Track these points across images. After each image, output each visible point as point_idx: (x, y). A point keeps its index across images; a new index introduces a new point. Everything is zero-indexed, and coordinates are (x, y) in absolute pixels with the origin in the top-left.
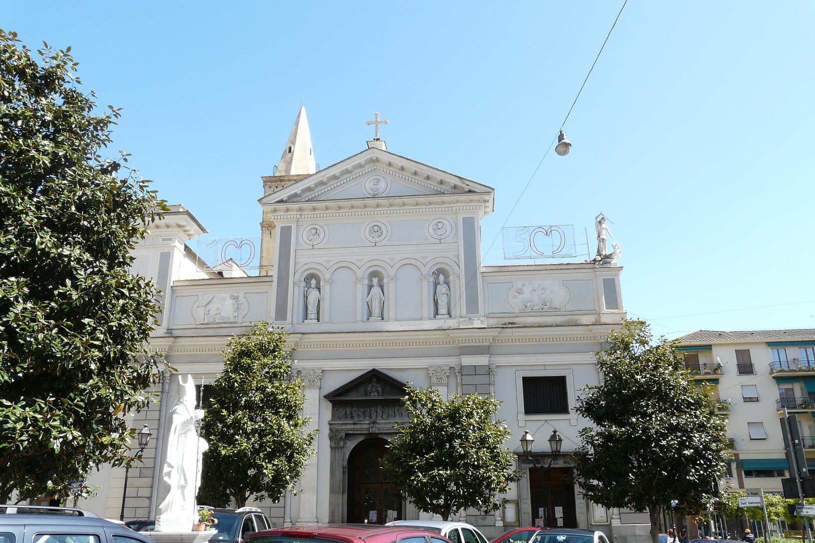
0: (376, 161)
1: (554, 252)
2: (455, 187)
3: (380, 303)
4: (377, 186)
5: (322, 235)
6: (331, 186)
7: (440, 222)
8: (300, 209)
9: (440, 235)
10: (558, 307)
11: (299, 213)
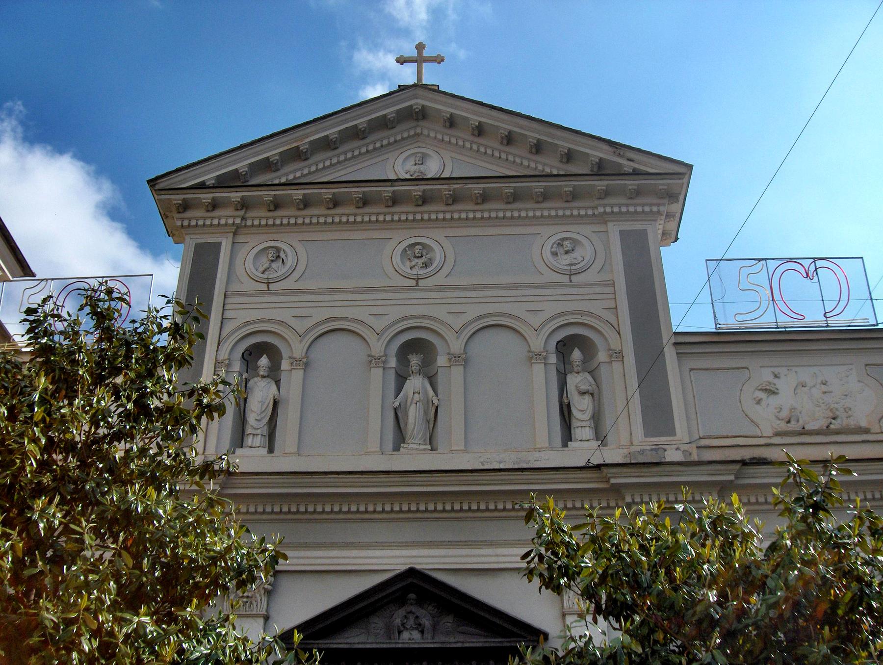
0: (421, 117)
1: (828, 315)
2: (601, 163)
3: (426, 413)
4: (422, 168)
5: (290, 262)
6: (190, 219)
7: (566, 239)
8: (244, 205)
9: (571, 265)
10: (864, 424)
11: (242, 213)
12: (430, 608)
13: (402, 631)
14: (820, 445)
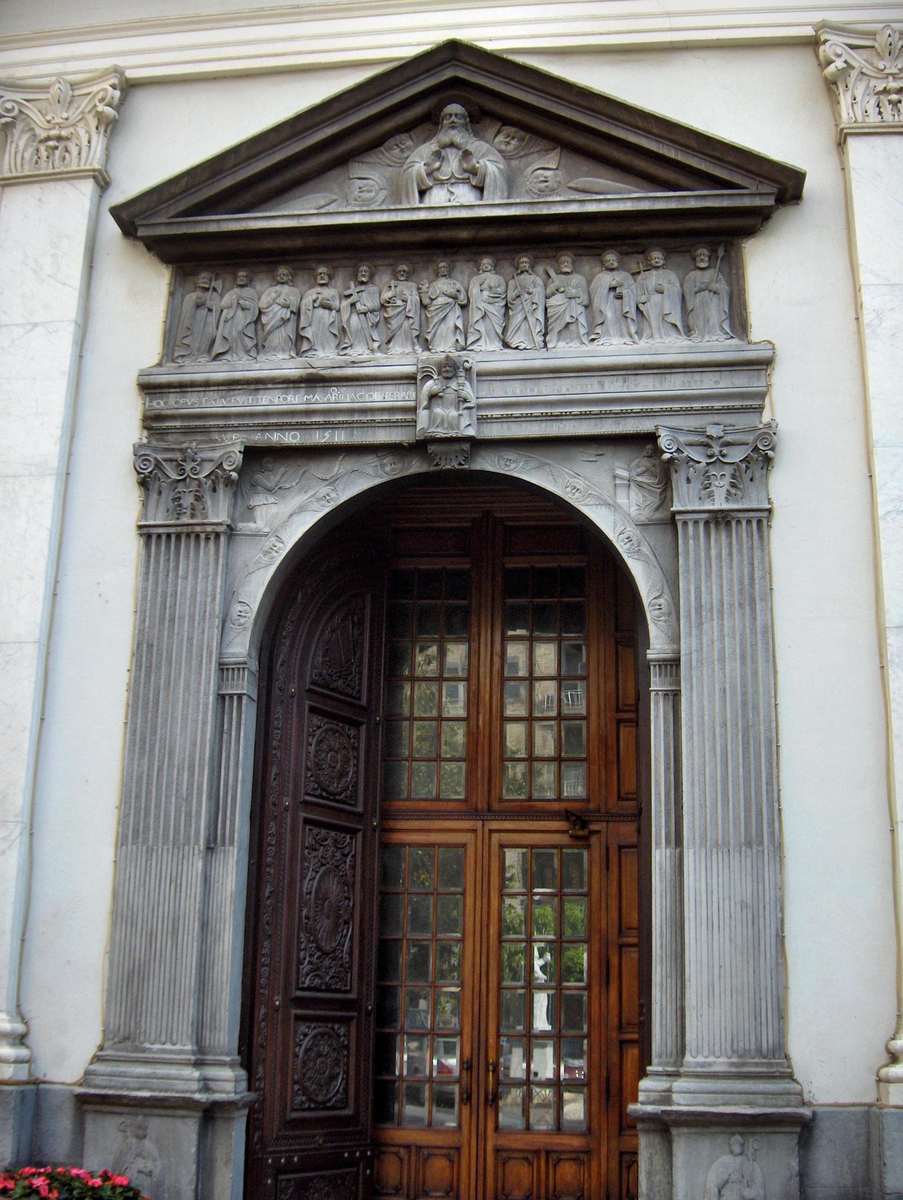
12: (500, 138)
13: (431, 188)
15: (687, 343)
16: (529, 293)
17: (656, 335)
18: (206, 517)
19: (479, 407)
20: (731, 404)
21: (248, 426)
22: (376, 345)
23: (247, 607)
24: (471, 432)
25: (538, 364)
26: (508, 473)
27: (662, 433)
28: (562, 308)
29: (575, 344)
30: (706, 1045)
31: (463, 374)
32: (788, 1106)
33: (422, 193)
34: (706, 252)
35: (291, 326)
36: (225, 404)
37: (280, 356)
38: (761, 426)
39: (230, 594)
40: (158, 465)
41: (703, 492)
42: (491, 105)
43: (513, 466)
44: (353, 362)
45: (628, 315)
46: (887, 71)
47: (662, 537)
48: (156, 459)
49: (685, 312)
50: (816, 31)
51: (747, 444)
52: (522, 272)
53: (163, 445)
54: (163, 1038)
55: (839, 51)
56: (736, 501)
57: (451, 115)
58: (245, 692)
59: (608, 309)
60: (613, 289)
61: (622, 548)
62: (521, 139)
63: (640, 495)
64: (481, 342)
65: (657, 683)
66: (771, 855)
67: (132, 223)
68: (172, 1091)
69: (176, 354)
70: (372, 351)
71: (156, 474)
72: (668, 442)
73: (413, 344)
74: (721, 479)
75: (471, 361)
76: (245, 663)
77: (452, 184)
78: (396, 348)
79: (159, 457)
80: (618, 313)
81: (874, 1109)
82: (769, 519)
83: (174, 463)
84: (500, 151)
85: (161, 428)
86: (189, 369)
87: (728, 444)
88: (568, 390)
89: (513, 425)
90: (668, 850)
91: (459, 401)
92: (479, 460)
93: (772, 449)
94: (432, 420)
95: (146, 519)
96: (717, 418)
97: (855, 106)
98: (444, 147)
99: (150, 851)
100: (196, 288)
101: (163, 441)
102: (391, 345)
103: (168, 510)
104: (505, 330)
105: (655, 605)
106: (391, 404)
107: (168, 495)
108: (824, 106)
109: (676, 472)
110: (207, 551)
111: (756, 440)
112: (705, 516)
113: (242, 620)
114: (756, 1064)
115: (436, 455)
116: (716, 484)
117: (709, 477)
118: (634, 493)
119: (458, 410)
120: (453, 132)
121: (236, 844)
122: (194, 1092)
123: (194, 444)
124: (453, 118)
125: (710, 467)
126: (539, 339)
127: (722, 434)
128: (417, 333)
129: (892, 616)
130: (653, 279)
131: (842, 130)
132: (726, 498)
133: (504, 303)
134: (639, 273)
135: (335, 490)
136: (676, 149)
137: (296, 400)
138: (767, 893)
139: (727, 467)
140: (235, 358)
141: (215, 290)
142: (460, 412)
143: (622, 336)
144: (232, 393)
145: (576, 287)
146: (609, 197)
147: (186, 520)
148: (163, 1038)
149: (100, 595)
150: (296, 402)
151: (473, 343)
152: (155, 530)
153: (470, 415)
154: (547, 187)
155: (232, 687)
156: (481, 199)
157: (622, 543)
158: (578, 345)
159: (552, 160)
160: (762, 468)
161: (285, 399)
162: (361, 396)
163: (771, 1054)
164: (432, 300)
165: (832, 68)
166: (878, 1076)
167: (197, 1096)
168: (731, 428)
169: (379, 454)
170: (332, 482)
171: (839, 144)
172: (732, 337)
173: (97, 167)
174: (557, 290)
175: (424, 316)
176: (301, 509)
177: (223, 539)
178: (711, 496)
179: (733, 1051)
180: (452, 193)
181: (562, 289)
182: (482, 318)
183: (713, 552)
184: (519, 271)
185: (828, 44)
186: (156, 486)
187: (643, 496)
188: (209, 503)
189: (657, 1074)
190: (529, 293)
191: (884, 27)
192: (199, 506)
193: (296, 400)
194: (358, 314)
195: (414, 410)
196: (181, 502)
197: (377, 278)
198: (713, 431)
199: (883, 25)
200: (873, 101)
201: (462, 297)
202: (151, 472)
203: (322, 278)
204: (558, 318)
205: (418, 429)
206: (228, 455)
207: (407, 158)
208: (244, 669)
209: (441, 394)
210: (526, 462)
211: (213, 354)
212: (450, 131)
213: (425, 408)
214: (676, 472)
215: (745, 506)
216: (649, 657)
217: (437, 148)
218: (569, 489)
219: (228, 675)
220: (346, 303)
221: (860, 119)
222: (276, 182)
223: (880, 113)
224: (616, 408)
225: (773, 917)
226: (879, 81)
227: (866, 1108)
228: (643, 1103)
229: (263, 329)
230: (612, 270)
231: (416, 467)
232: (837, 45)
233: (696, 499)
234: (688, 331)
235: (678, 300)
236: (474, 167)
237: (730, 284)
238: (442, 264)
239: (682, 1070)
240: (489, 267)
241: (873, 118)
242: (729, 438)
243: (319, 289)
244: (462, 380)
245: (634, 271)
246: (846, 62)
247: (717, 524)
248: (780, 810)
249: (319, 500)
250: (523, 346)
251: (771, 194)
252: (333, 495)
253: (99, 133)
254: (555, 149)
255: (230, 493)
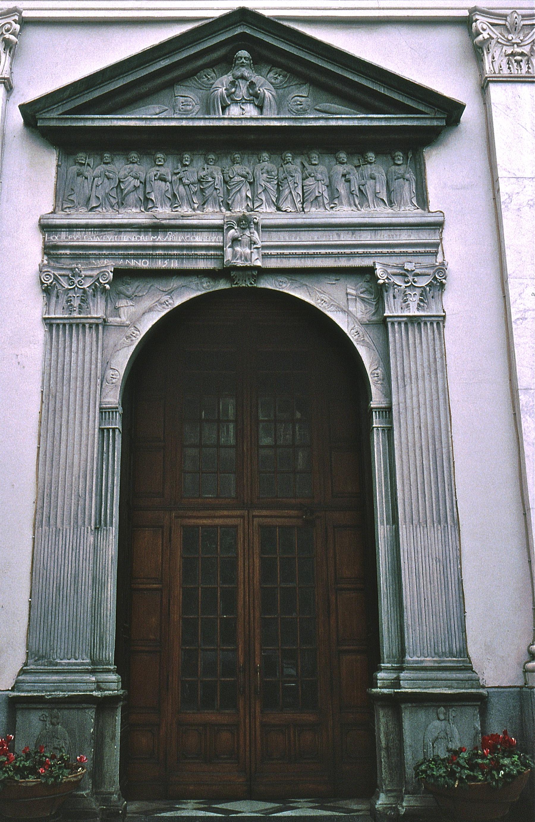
12: (271, 74)
13: (229, 105)
14: (501, 300)
15: (390, 211)
16: (292, 176)
17: (371, 205)
18: (90, 313)
19: (264, 247)
20: (418, 250)
21: (115, 254)
22: (196, 206)
23: (117, 372)
24: (259, 263)
25: (299, 221)
26: (281, 290)
27: (378, 266)
28: (314, 186)
29: (322, 210)
30: (419, 649)
31: (253, 226)
32: (472, 688)
33: (224, 109)
34: (401, 154)
35: (141, 191)
36: (99, 240)
37: (134, 210)
38: (437, 264)
39: (106, 364)
40: (56, 278)
41: (404, 304)
42: (266, 53)
43: (284, 285)
44: (182, 216)
45: (354, 192)
46: (514, 41)
47: (374, 332)
48: (54, 274)
49: (389, 192)
50: (470, 13)
51: (430, 275)
52: (287, 163)
53: (58, 265)
54: (69, 656)
55: (485, 27)
56: (423, 310)
57: (241, 58)
58: (117, 427)
59: (342, 188)
60: (344, 175)
61: (353, 338)
62: (285, 76)
63: (363, 305)
64: (263, 206)
65: (377, 422)
66: (453, 528)
67: (34, 117)
68: (77, 691)
69: (65, 206)
70: (194, 210)
71: (55, 284)
72: (382, 273)
73: (220, 206)
74: (414, 296)
75: (258, 218)
76: (118, 408)
77: (243, 103)
78: (209, 209)
79: (56, 273)
80: (348, 191)
81: (524, 689)
82: (444, 322)
83: (66, 278)
84: (272, 83)
85: (56, 254)
86: (74, 217)
87: (417, 275)
88: (318, 238)
89: (284, 260)
90: (388, 526)
91: (251, 244)
92: (262, 281)
93: (445, 279)
94: (234, 255)
95: (49, 314)
96: (409, 258)
97: (494, 63)
98: (237, 78)
99: (58, 531)
100: (76, 163)
101: (57, 263)
102: (205, 206)
103: (63, 308)
104: (278, 199)
105: (374, 374)
106: (207, 244)
107: (63, 300)
108: (472, 67)
109: (387, 291)
110: (89, 336)
111: (434, 273)
112: (404, 319)
113: (114, 381)
114: (450, 661)
115: (236, 277)
116: (411, 299)
117: (406, 295)
118: (360, 306)
119: (251, 249)
120: (243, 69)
121: (114, 525)
122: (92, 691)
123: (80, 265)
124: (243, 60)
125: (407, 289)
126: (299, 205)
127: (414, 268)
128: (222, 199)
129: (522, 381)
130: (368, 170)
131: (487, 78)
132: (417, 308)
133: (276, 182)
134: (359, 166)
135: (171, 298)
136: (384, 87)
137: (146, 240)
138: (451, 552)
139: (417, 289)
140: (104, 210)
141: (88, 165)
142: (252, 250)
143: (350, 205)
144: (103, 233)
145: (321, 173)
146: (343, 116)
147: (76, 315)
148: (69, 656)
149: (19, 363)
150: (146, 240)
151: (257, 207)
152: (54, 321)
153: (258, 252)
154: (301, 108)
155: (109, 424)
156: (261, 114)
157: (353, 335)
158: (324, 210)
159: (304, 91)
160: (439, 290)
161: (139, 238)
162: (188, 238)
163: (458, 654)
164: (231, 178)
165: (480, 37)
166: (524, 668)
167: (95, 693)
168: (419, 265)
169: (199, 276)
170: (170, 293)
171: (482, 88)
172: (418, 208)
173: (6, 76)
174: (310, 175)
175: (225, 188)
176: (151, 310)
177: (100, 328)
178: (408, 306)
179: (435, 653)
180: (243, 109)
181: (313, 175)
182: (263, 191)
183: (411, 341)
184: (285, 162)
185: (478, 22)
186: (55, 292)
187: (365, 306)
188: (91, 304)
189: (387, 669)
190: (292, 176)
191: (512, 12)
192: (84, 306)
193: (146, 240)
194: (184, 186)
195: (221, 248)
196: (72, 303)
197: (195, 162)
198: (408, 266)
199: (512, 10)
200: (505, 60)
201: (250, 177)
202: (51, 283)
203: (160, 161)
204: (311, 193)
205: (225, 260)
206: (103, 274)
207: (212, 84)
208: (116, 412)
209: (240, 238)
210: (292, 284)
211: (90, 208)
212: (240, 68)
213: (229, 247)
214: (387, 291)
215: (429, 314)
216: (372, 406)
217: (232, 79)
218: (319, 301)
219: (105, 416)
220: (175, 178)
221: (497, 72)
222: (129, 95)
223: (509, 68)
224: (348, 251)
225: (456, 568)
226: (508, 47)
227: (519, 689)
228: (380, 688)
229: (122, 193)
230: (343, 163)
231: (223, 285)
232: (483, 23)
233: (399, 309)
234: (391, 203)
235: (385, 183)
236: (257, 92)
237: (416, 175)
238: (236, 156)
239: (405, 665)
240: (267, 159)
241: (505, 72)
242: (417, 271)
243: (157, 168)
244: (253, 230)
245: (357, 165)
246: (488, 34)
247: (412, 323)
248: (40, 425)
249: (161, 304)
250: (289, 210)
251: (443, 118)
252: (171, 301)
253: (6, 53)
254: (306, 84)
255: (104, 297)
